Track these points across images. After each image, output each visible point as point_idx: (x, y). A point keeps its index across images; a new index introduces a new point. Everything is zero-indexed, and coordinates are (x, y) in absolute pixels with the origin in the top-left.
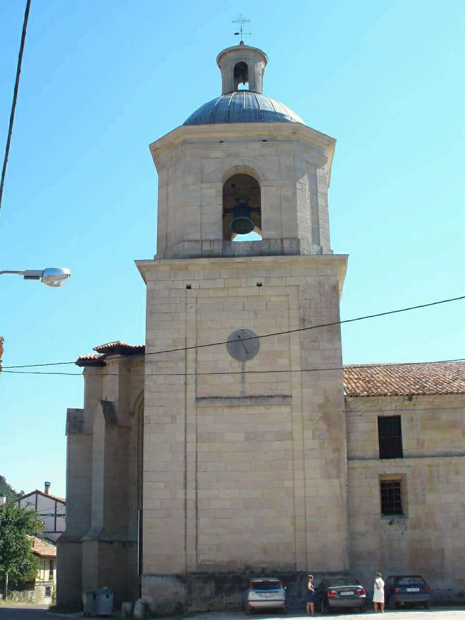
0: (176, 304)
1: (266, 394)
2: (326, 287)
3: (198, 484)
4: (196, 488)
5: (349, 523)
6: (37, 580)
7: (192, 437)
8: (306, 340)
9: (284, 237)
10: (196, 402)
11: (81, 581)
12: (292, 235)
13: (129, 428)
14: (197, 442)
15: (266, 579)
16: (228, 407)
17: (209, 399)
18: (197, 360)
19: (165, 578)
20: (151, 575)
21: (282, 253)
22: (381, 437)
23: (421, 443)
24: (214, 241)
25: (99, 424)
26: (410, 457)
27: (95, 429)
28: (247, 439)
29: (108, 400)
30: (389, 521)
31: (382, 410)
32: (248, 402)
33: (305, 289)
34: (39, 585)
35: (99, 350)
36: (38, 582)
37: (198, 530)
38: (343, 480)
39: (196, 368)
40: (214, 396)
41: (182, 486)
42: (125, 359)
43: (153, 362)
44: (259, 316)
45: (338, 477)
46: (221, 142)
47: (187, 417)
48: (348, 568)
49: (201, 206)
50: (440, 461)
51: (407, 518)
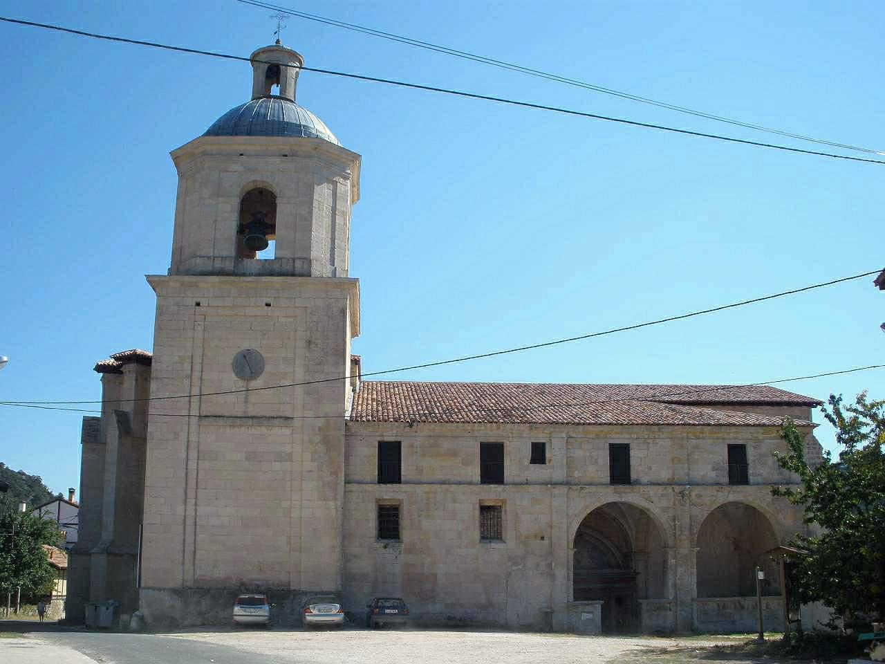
1: (268, 415)
2: (335, 310)
5: (343, 546)
6: (54, 593)
9: (297, 256)
12: (305, 255)
14: (198, 460)
15: (251, 596)
19: (162, 591)
20: (149, 588)
21: (293, 275)
23: (420, 470)
24: (226, 257)
25: (112, 435)
26: (407, 483)
28: (247, 459)
30: (383, 545)
32: (250, 422)
35: (116, 359)
36: (55, 596)
38: (339, 503)
45: (335, 499)
46: (242, 155)
48: (340, 588)
50: (438, 488)
51: (402, 542)
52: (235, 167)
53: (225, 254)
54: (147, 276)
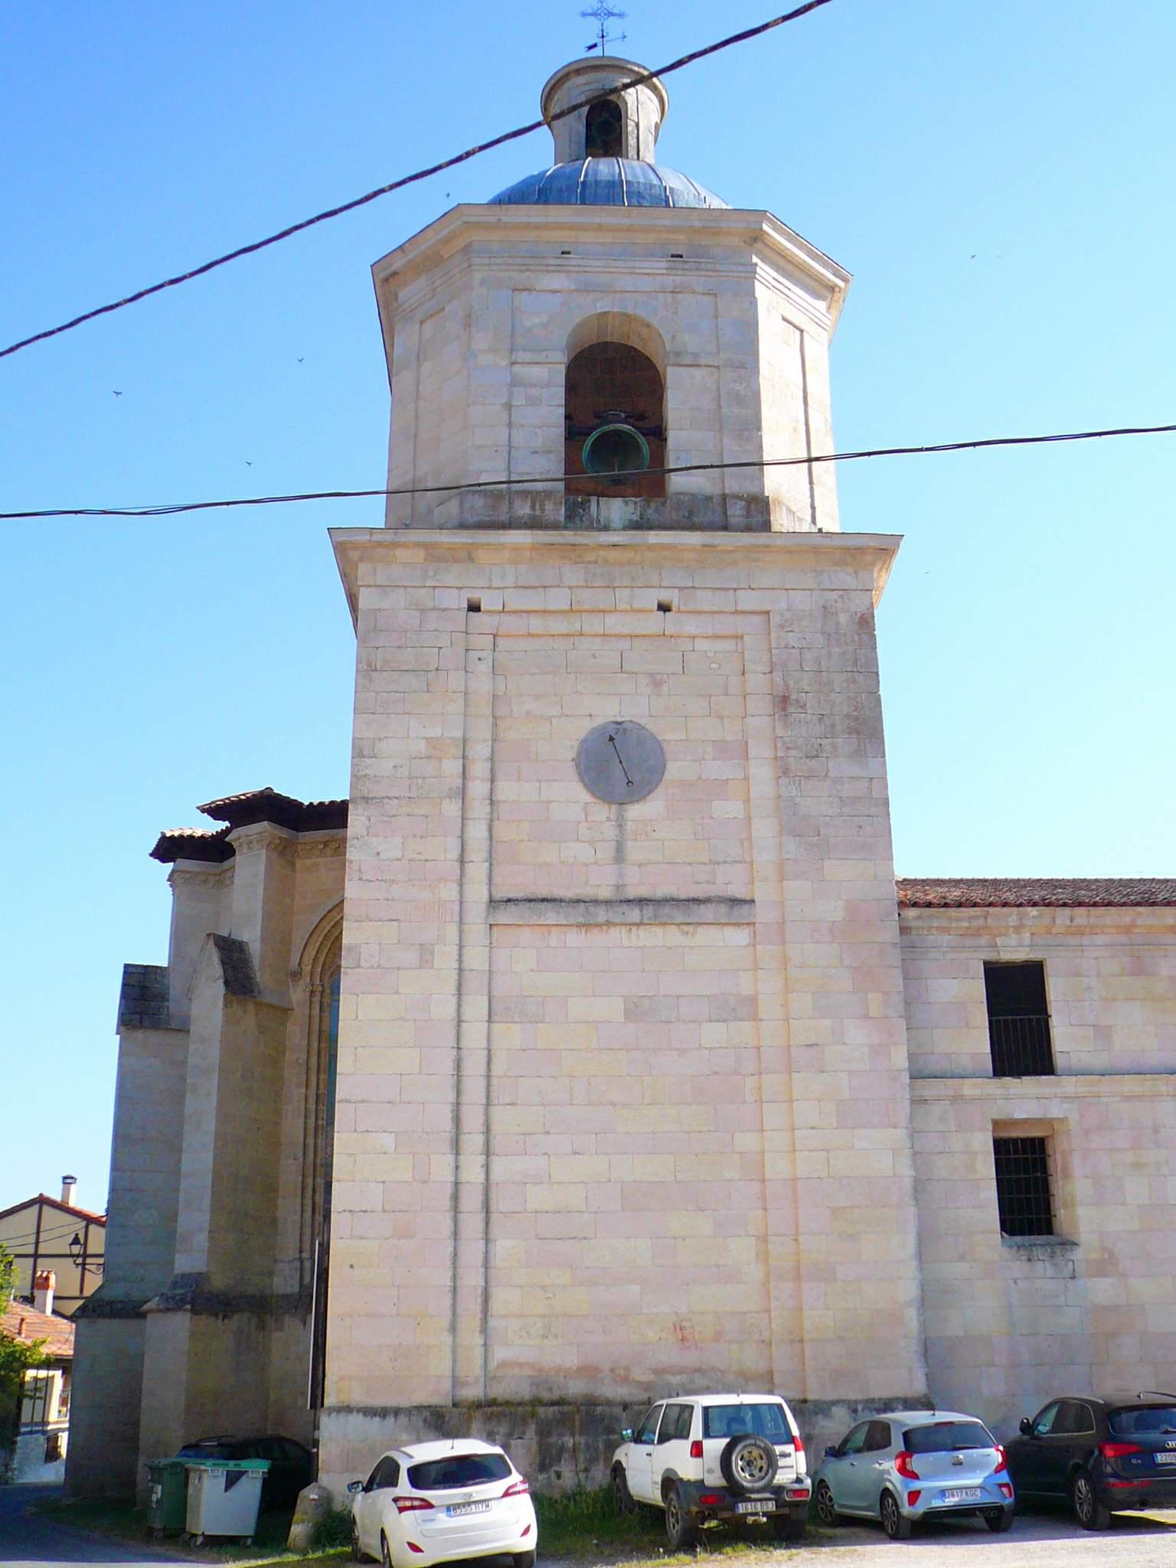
0: (440, 648)
3: (491, 1138)
4: (488, 1152)
7: (476, 1007)
8: (792, 752)
10: (488, 912)
11: (136, 1424)
13: (285, 1011)
14: (490, 1021)
16: (579, 926)
17: (528, 905)
18: (494, 799)
20: (347, 1409)
22: (993, 1018)
27: (195, 1010)
28: (635, 1011)
29: (232, 937)
31: (996, 946)
32: (634, 914)
33: (787, 620)
34: (31, 1433)
35: (215, 811)
37: (492, 1271)
39: (491, 820)
40: (540, 897)
41: (446, 1146)
42: (284, 833)
43: (372, 799)
44: (665, 688)
47: (465, 951)
49: (509, 407)
52: (557, 281)
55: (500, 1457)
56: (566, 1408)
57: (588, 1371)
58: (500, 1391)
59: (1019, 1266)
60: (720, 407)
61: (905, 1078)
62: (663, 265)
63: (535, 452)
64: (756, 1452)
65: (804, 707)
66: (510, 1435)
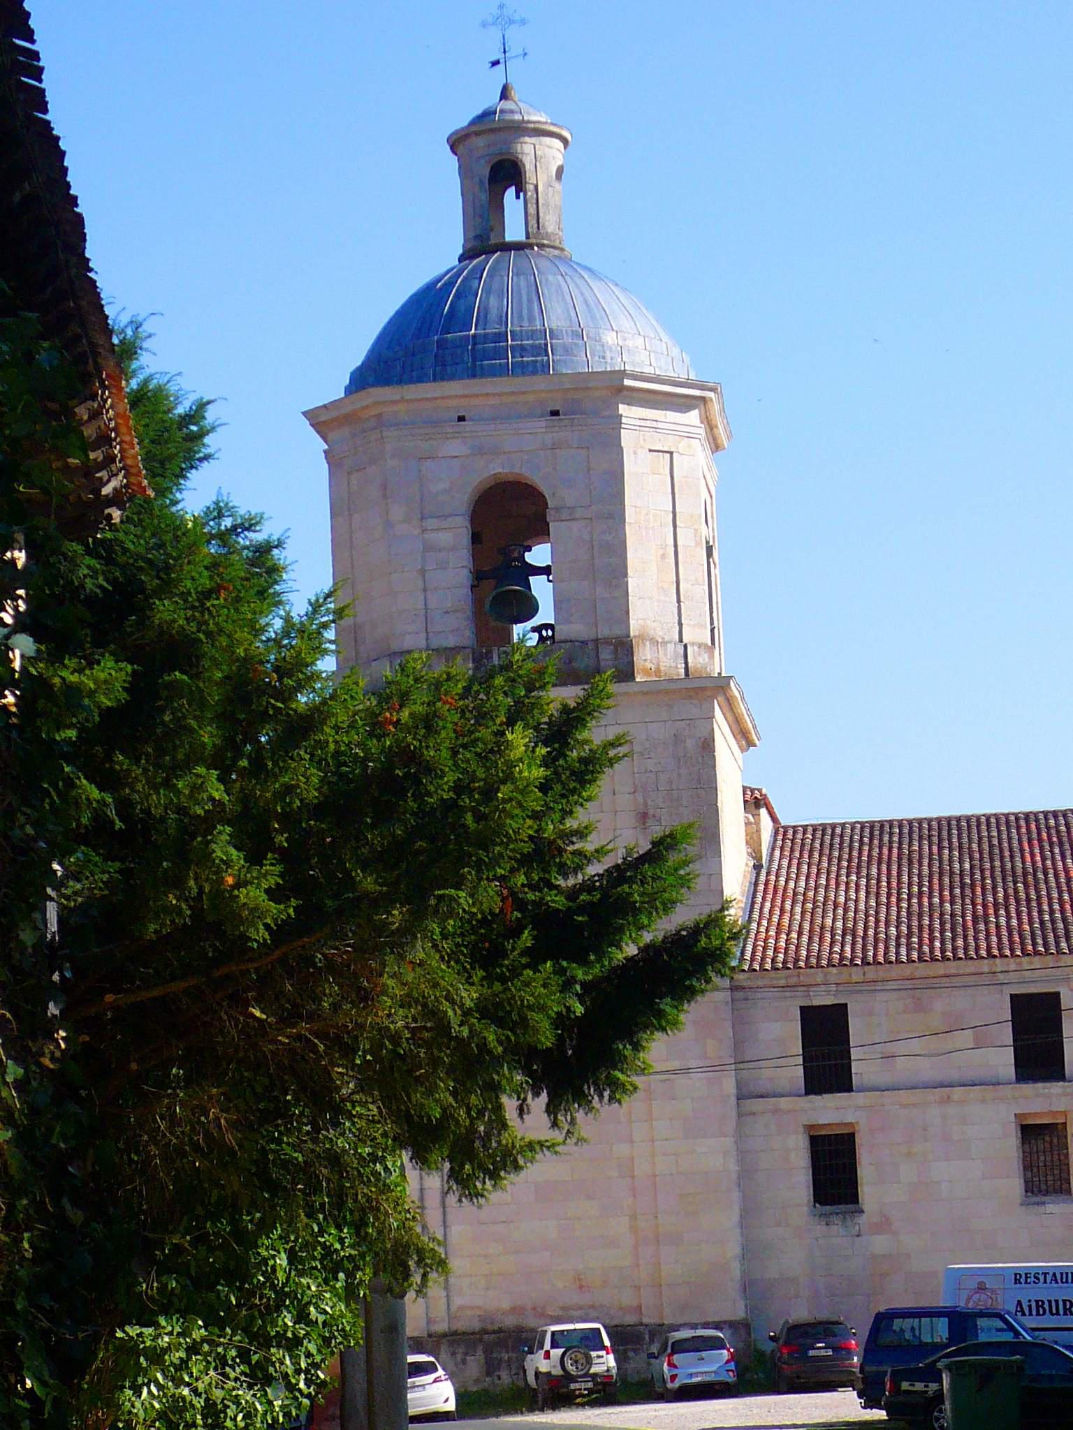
2: (689, 743)
12: (617, 631)
26: (862, 1090)
49: (423, 572)
52: (455, 447)
53: (451, 642)
54: (304, 414)
55: (433, 1363)
56: (502, 1335)
57: (516, 1310)
58: (460, 1326)
59: (820, 1229)
60: (593, 558)
61: (733, 1100)
62: (544, 424)
63: (447, 612)
64: (579, 1356)
65: (659, 820)
66: (466, 1354)
